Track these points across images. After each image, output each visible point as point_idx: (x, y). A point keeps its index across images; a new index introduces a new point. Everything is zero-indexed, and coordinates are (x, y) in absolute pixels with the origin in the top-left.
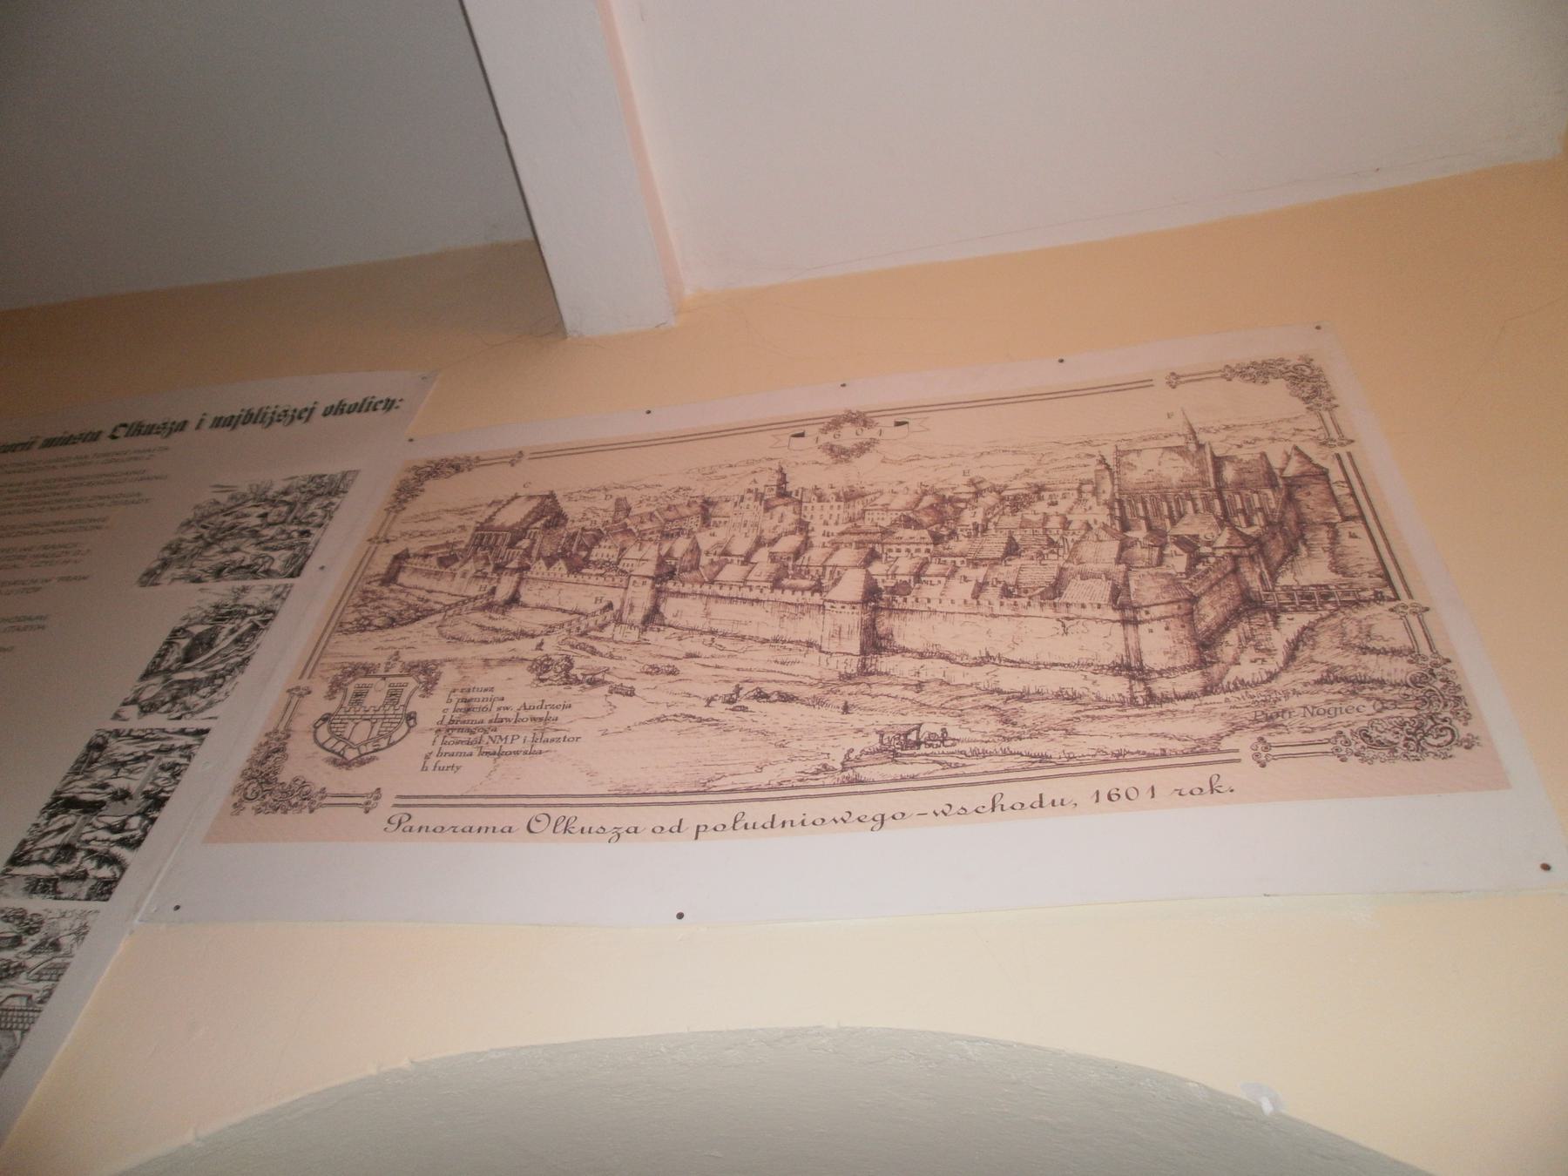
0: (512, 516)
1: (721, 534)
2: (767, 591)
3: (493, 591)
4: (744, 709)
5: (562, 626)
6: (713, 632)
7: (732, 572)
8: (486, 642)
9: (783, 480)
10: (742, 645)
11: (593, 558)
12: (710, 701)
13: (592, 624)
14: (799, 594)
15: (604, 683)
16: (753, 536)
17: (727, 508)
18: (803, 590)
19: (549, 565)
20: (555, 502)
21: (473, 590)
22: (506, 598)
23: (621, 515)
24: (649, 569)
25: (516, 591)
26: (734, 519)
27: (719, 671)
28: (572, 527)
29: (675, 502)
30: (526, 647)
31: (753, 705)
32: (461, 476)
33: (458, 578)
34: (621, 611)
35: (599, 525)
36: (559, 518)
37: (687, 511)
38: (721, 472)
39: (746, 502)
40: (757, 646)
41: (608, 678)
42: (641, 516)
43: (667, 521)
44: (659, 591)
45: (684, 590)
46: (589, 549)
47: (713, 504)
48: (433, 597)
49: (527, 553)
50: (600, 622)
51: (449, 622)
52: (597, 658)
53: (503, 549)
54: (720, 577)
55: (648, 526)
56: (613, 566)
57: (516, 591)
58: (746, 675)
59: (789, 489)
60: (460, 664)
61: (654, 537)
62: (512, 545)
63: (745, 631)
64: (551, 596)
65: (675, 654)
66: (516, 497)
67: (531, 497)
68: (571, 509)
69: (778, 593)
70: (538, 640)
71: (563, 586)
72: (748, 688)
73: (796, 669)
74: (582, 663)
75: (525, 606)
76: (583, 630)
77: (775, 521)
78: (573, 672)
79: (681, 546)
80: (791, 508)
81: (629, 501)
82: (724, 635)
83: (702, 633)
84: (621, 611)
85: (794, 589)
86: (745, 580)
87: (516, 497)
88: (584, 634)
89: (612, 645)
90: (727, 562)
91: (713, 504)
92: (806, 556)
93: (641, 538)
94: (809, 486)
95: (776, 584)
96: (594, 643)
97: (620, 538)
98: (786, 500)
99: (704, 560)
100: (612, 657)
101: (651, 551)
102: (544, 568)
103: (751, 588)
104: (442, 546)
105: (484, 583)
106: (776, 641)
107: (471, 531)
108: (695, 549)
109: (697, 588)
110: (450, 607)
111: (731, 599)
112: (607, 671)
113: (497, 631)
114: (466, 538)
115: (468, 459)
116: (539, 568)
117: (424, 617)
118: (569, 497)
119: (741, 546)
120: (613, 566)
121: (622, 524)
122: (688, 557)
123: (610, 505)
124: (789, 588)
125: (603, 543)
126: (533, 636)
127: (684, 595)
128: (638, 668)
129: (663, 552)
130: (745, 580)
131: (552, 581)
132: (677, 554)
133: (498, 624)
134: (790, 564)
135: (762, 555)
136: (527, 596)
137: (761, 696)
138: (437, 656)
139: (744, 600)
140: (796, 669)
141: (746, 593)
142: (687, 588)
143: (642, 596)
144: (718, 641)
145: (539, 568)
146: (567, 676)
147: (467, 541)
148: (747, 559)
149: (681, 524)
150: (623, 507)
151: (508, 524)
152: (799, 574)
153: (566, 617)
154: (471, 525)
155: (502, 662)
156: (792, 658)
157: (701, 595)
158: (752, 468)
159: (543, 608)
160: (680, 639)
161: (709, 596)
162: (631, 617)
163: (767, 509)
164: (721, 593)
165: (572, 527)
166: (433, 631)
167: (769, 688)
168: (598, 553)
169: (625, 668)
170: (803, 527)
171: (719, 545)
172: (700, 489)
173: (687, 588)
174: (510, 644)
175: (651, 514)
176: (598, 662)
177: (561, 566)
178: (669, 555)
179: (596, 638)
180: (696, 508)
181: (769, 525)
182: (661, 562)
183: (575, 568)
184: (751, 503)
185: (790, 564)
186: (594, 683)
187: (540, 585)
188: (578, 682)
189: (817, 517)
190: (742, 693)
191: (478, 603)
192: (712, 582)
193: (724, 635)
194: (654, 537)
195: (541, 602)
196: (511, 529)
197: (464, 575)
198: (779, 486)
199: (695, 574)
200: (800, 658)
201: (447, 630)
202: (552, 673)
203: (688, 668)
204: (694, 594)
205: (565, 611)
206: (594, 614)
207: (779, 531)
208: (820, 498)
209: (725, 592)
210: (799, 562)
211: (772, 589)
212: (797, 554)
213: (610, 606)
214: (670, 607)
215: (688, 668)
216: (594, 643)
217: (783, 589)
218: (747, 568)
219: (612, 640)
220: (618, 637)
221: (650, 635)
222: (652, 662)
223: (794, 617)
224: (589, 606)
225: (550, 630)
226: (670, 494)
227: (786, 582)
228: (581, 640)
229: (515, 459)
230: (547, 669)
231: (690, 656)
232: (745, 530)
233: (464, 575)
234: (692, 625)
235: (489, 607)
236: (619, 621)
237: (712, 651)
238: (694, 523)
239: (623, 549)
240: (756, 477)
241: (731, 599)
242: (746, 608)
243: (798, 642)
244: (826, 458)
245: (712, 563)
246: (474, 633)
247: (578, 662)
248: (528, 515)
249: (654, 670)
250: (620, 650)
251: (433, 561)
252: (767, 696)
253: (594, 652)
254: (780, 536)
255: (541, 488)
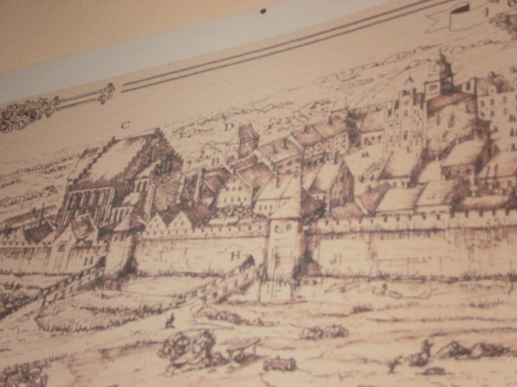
0: (112, 166)
1: (376, 152)
2: (446, 217)
3: (102, 262)
4: (440, 371)
5: (194, 293)
6: (382, 277)
7: (397, 198)
8: (100, 328)
9: (448, 72)
10: (425, 288)
11: (221, 205)
12: (393, 365)
13: (231, 287)
14: (488, 215)
15: (256, 358)
16: (417, 149)
17: (380, 119)
18: (493, 209)
19: (168, 221)
20: (163, 141)
21: (77, 265)
22: (120, 268)
23: (248, 147)
24: (292, 208)
25: (131, 259)
26: (390, 132)
27: (399, 326)
28: (189, 170)
29: (314, 120)
30: (153, 327)
31: (449, 365)
32: (37, 122)
33: (55, 251)
34: (264, 265)
35: (222, 163)
36: (170, 161)
37: (329, 131)
38: (365, 76)
39: (402, 108)
40: (443, 288)
41: (260, 351)
42: (272, 144)
43: (306, 146)
44: (308, 234)
45: (339, 229)
46: (215, 195)
47: (362, 116)
48: (25, 281)
49: (139, 209)
50: (241, 282)
51: (50, 309)
52: (243, 328)
53: (108, 208)
54: (383, 207)
55: (283, 155)
56: (247, 211)
57: (131, 259)
58: (435, 326)
59: (456, 83)
60: (71, 361)
61: (292, 168)
62: (117, 202)
63: (424, 270)
64: (175, 258)
65: (340, 311)
66: (114, 142)
67: (132, 140)
68: (184, 147)
69: (460, 218)
70: (165, 317)
71: (189, 244)
72: (439, 344)
73: (500, 312)
74: (225, 336)
75: (144, 275)
76: (222, 298)
77: (444, 126)
78: (215, 349)
79: (327, 174)
80: (462, 106)
81: (256, 128)
82: (398, 279)
83: (370, 279)
84: (264, 265)
85: (481, 210)
86: (415, 207)
87: (114, 142)
88: (223, 300)
89: (259, 309)
90: (388, 187)
91: (362, 116)
92: (492, 164)
93: (277, 171)
94: (484, 74)
95: (456, 205)
96: (238, 310)
97: (251, 176)
98: (455, 97)
99: (359, 189)
100: (261, 324)
101: (292, 187)
102: (162, 226)
103: (386, 218)
104: (28, 216)
105: (85, 254)
106: (467, 278)
107: (62, 192)
108: (346, 177)
109: (355, 224)
110: (49, 290)
111: (400, 232)
112: (258, 342)
113: (112, 311)
114: (57, 200)
115: (44, 102)
116: (156, 225)
117: (16, 308)
118: (181, 133)
119: (403, 164)
120: (247, 211)
121: (250, 157)
122: (339, 188)
123: (232, 135)
124: (475, 208)
125: (230, 185)
126: (160, 312)
127: (340, 235)
128: (296, 333)
129: (307, 185)
130: (415, 207)
131: (173, 240)
132: (325, 185)
133: (113, 304)
134: (472, 178)
135: (432, 172)
136: (145, 262)
137: (459, 352)
138: (39, 356)
139: (417, 231)
140: (500, 312)
141: (417, 222)
142: (342, 226)
143: (288, 244)
144: (392, 287)
145: (156, 225)
146: (209, 356)
147: (59, 205)
148: (413, 179)
149: (325, 147)
150: (248, 137)
151: (109, 177)
152: (484, 189)
153: (198, 282)
154: (62, 184)
155: (125, 350)
156: (493, 298)
157: (362, 232)
158: (406, 63)
159: (168, 274)
160: (343, 290)
161: (371, 232)
162: (279, 271)
163: (430, 113)
164: (386, 226)
165: (189, 170)
166: (31, 324)
167: (467, 341)
168: (227, 198)
169: (280, 335)
170: (481, 128)
171: (374, 166)
172: (341, 101)
173: (342, 226)
174: (132, 326)
175: (285, 140)
176: (243, 333)
177: (182, 220)
178: (314, 187)
179: (239, 303)
180: (340, 125)
181: (435, 132)
182: (306, 197)
183: (200, 221)
184: (410, 108)
185: (472, 178)
186: (243, 360)
187: (160, 246)
188: (223, 361)
189: (499, 112)
190: (433, 351)
191: (85, 280)
192: (372, 214)
193: (398, 279)
194: (292, 168)
195: (164, 268)
196: (113, 182)
197: (61, 248)
198: (443, 82)
199: (350, 207)
200: (504, 297)
201: (49, 320)
202: (189, 355)
203: (359, 326)
204: (352, 231)
205: (195, 275)
206: (232, 273)
207: (450, 138)
208: (501, 88)
209: (391, 224)
210: (483, 174)
211: (452, 212)
212: (479, 164)
213: (250, 261)
214: (325, 253)
215: (359, 326)
216: (238, 310)
217: (466, 211)
218: (415, 190)
219: (258, 302)
220: (265, 298)
221: (305, 291)
222: (313, 323)
223: (486, 246)
224: (225, 264)
225: (180, 300)
226: (305, 111)
227: (468, 201)
228: (221, 308)
229: (105, 94)
230: (182, 350)
231: (358, 310)
232: (405, 144)
233: (61, 248)
234: (355, 271)
235: (99, 282)
236: (263, 278)
237: (387, 300)
238: (339, 143)
239: (256, 189)
240: (413, 73)
241: (400, 232)
242: (421, 241)
243: (498, 277)
244: (503, 34)
245: (370, 190)
246: (85, 319)
247: (220, 336)
248: (133, 162)
249: (317, 334)
250: (270, 314)
251: (20, 235)
252: (467, 352)
253: (238, 320)
254: (452, 145)
255: (144, 126)
